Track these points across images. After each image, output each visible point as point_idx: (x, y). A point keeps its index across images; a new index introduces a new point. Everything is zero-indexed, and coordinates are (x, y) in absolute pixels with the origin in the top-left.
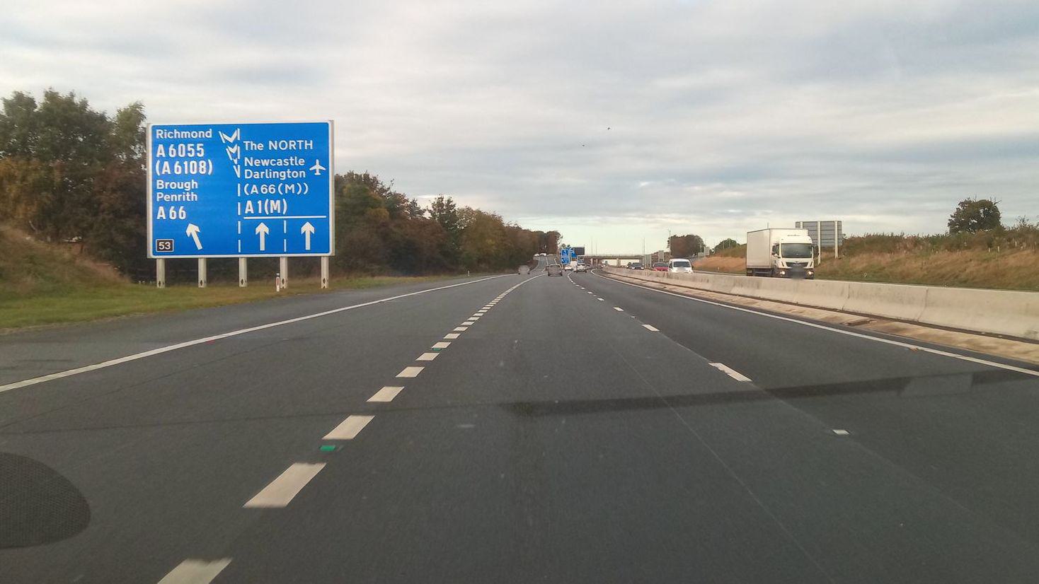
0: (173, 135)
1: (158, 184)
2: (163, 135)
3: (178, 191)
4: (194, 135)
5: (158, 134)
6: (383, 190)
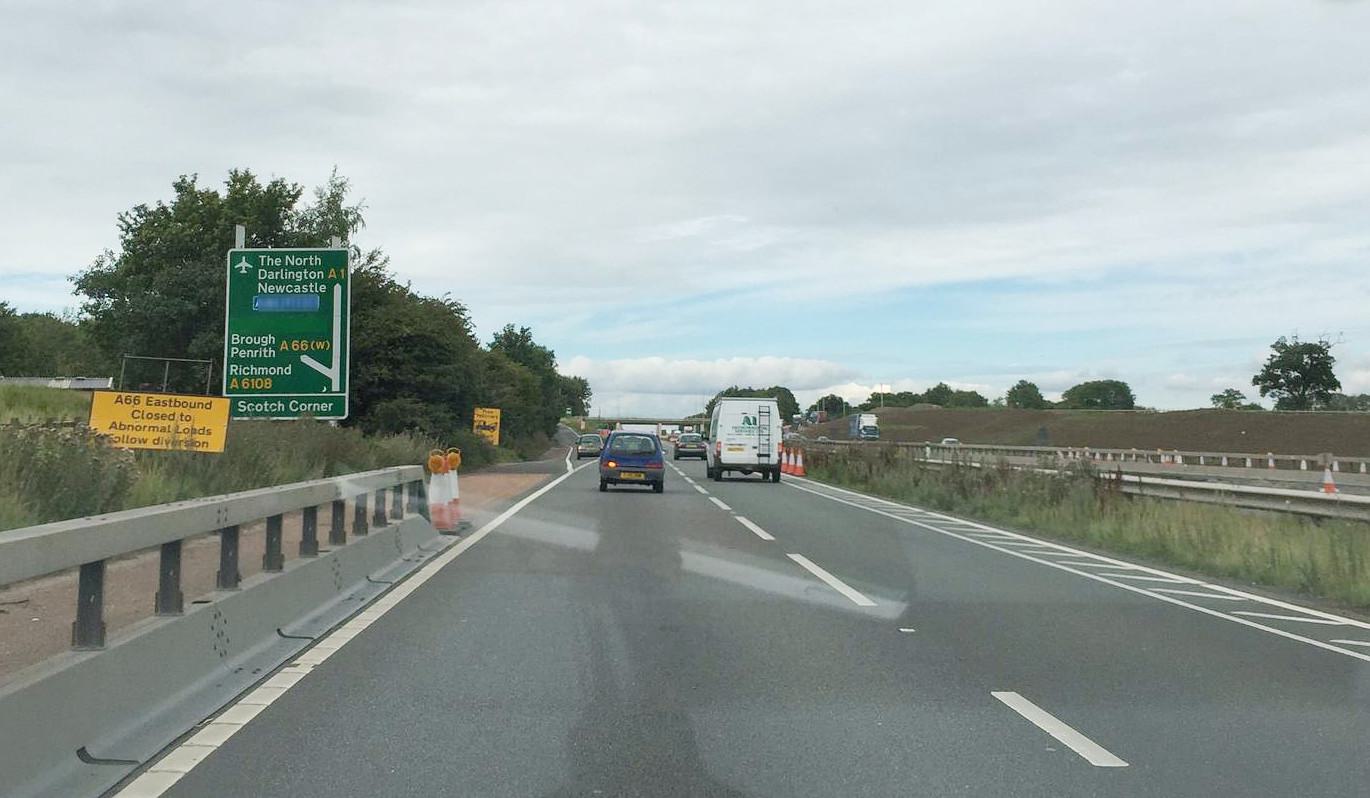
0: (250, 371)
1: (233, 339)
2: (238, 371)
3: (254, 347)
4: (272, 371)
5: (232, 370)
6: (537, 347)
